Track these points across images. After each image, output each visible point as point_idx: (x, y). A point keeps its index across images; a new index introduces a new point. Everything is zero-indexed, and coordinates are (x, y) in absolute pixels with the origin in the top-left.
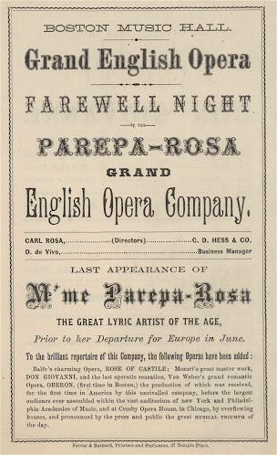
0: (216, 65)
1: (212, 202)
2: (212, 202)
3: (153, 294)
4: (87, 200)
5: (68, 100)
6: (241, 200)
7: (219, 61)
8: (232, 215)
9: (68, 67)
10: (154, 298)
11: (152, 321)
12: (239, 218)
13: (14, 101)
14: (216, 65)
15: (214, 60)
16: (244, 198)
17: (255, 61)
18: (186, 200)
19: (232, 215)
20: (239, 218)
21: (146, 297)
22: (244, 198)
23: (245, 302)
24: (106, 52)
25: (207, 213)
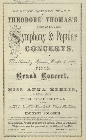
0: (29, 21)
1: (71, 36)
2: (71, 36)
3: (59, 75)
4: (35, 35)
5: (75, 22)
6: (44, 35)
7: (21, 20)
8: (42, 40)
9: (15, 18)
10: (59, 77)
11: (32, 113)
12: (23, 41)
13: (80, 21)
14: (29, 21)
15: (28, 20)
16: (45, 35)
17: (7, 20)
18: (39, 35)
19: (42, 40)
20: (23, 41)
21: (57, 77)
22: (45, 35)
23: (52, 75)
24: (18, 18)
25: (64, 39)
